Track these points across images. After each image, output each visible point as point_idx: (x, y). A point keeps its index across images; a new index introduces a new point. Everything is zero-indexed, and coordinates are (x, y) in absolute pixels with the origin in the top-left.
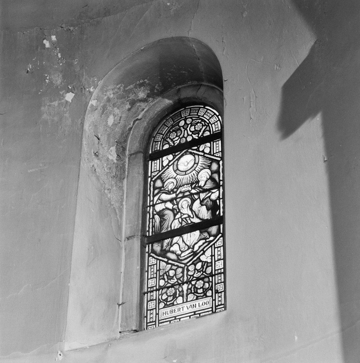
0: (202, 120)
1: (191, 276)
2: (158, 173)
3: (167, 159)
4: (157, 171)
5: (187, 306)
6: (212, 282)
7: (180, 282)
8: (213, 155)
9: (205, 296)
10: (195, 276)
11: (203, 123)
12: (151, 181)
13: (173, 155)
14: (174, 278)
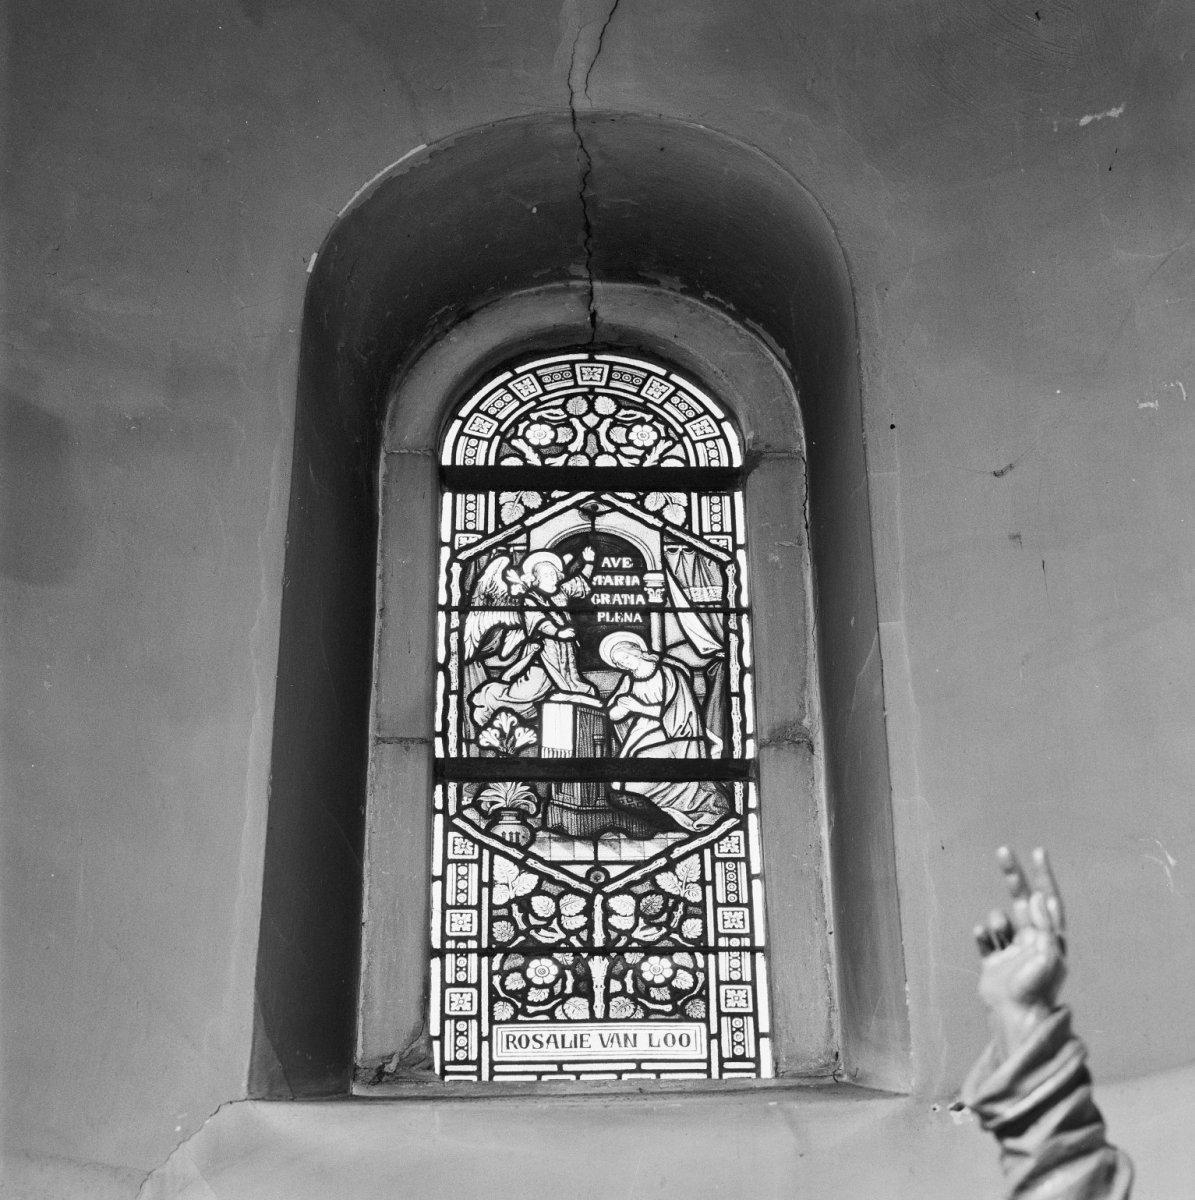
0: (657, 417)
1: (621, 933)
2: (479, 542)
3: (521, 502)
4: (474, 531)
5: (601, 1035)
6: (705, 971)
7: (577, 944)
8: (700, 537)
9: (677, 1016)
10: (637, 934)
11: (661, 427)
12: (453, 558)
13: (543, 496)
14: (552, 926)
